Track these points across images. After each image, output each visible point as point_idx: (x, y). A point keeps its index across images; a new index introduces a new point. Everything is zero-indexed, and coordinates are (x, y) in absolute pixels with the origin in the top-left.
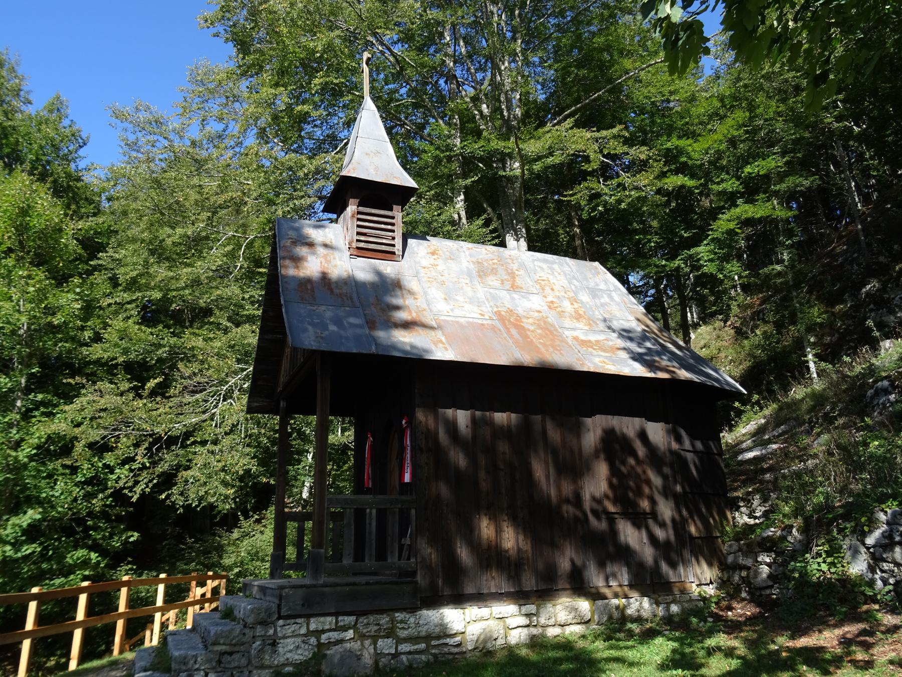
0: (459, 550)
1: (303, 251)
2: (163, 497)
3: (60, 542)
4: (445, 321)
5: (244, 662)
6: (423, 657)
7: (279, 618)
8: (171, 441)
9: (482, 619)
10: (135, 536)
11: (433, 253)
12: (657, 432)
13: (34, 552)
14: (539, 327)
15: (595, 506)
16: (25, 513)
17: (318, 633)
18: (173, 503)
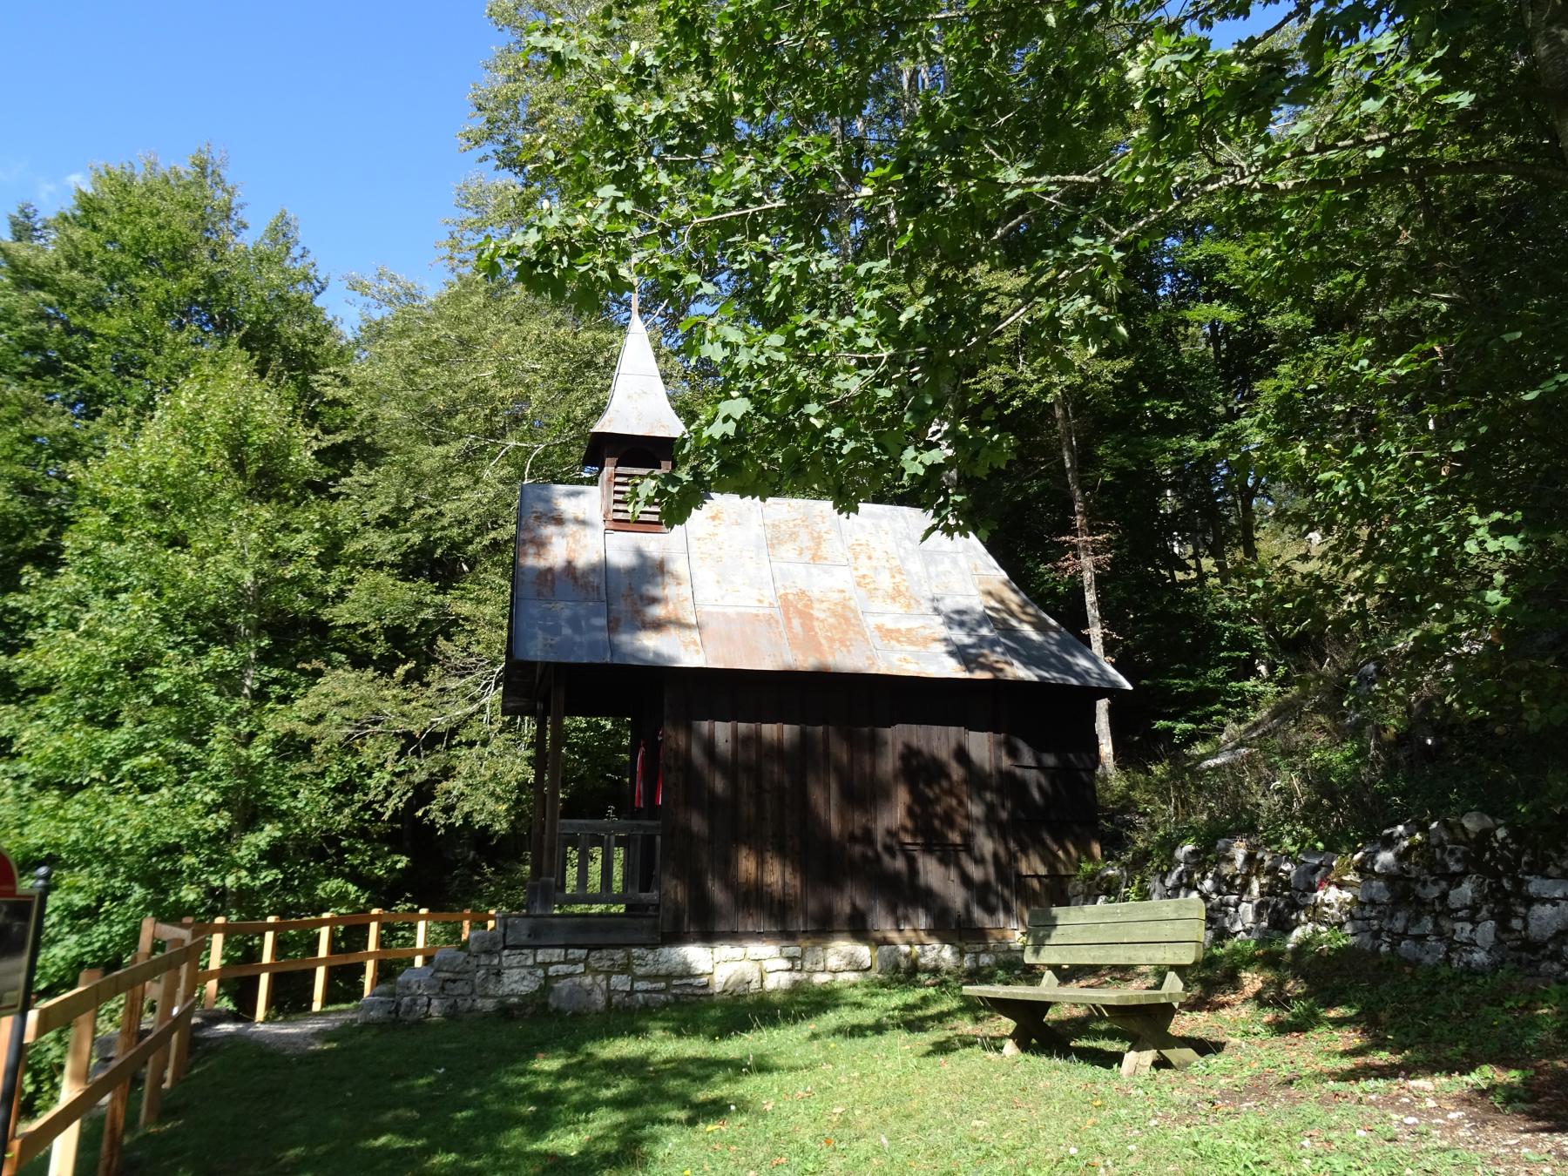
0: (710, 884)
1: (549, 530)
2: (420, 813)
3: (308, 868)
4: (709, 614)
5: (467, 990)
6: (662, 997)
7: (505, 948)
8: (433, 739)
9: (734, 960)
10: (403, 862)
11: (714, 518)
12: (981, 746)
13: (275, 880)
14: (834, 614)
15: (888, 840)
16: (262, 830)
17: (545, 965)
18: (433, 822)
